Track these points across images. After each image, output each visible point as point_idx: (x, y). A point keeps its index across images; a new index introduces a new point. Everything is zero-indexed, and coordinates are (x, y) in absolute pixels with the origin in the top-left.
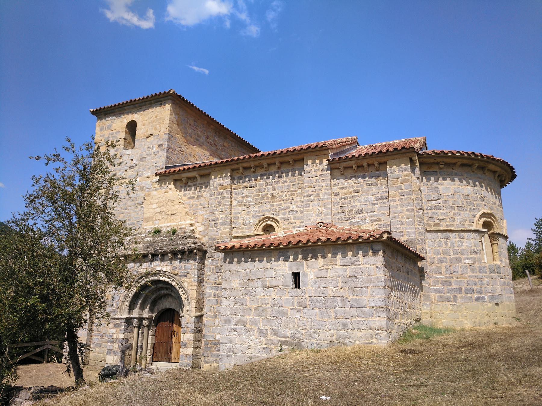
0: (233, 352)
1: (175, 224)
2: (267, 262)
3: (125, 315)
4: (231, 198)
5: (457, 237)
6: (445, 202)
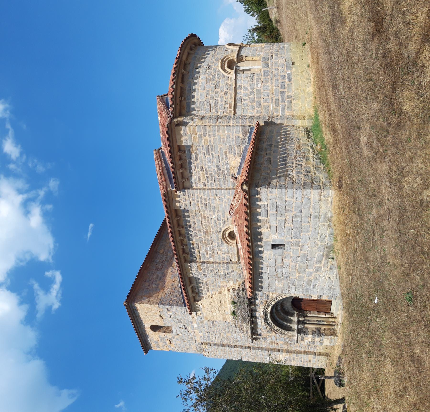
0: (331, 288)
1: (228, 301)
2: (263, 265)
3: (295, 333)
4: (207, 263)
5: (240, 91)
6: (212, 98)
